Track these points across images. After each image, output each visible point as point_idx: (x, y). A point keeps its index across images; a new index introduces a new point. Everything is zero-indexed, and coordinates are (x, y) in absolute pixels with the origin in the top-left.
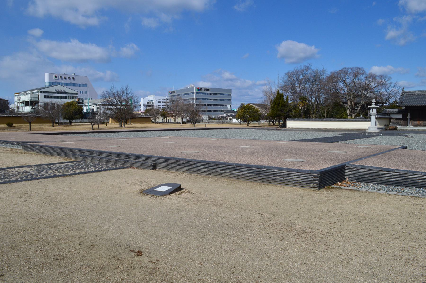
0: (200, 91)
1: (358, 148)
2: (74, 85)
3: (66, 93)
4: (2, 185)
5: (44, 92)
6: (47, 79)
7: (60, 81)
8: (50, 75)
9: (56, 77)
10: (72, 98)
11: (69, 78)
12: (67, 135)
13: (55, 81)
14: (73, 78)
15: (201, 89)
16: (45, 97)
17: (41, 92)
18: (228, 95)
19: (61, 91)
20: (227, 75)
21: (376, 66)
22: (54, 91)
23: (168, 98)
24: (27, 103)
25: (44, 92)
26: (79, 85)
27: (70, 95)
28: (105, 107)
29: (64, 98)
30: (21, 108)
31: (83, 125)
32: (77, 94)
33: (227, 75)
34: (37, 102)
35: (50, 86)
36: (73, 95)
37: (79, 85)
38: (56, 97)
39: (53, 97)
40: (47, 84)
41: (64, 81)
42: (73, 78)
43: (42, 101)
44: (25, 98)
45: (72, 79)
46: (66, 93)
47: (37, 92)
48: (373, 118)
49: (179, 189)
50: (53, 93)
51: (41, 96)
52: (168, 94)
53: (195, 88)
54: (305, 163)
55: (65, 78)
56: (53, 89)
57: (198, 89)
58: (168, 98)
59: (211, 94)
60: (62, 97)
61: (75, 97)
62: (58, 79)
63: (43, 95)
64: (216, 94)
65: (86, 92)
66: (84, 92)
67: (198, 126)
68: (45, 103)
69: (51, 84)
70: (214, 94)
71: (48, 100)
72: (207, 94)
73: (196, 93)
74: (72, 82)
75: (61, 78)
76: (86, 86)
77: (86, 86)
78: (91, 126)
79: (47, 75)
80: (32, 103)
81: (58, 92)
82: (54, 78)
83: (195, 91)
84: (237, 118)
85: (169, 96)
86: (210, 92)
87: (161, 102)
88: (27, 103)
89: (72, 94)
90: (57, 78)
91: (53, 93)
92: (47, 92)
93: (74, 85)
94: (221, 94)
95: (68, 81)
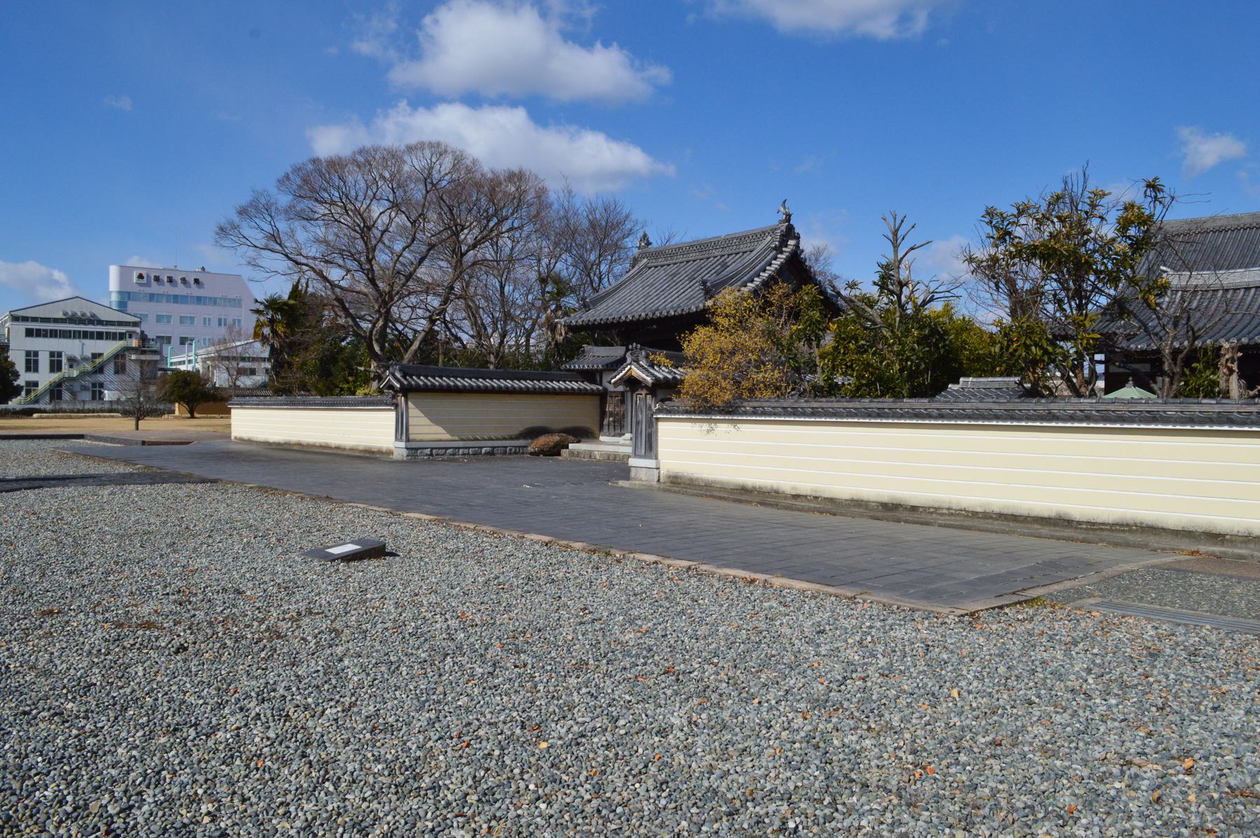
2: (199, 300)
3: (100, 322)
4: (1257, 532)
5: (25, 319)
6: (114, 285)
8: (125, 271)
9: (141, 276)
10: (122, 336)
13: (137, 289)
14: (197, 281)
16: (29, 333)
19: (84, 315)
22: (60, 315)
25: (25, 319)
26: (214, 301)
27: (112, 329)
29: (92, 338)
31: (71, 418)
36: (123, 329)
37: (214, 301)
39: (54, 334)
42: (197, 281)
46: (100, 322)
48: (273, 190)
60: (86, 335)
62: (148, 284)
63: (22, 327)
71: (44, 346)
74: (195, 291)
78: (133, 422)
79: (114, 271)
82: (135, 279)
89: (120, 324)
90: (145, 281)
91: (56, 321)
92: (35, 319)
93: (199, 300)
95: (180, 290)
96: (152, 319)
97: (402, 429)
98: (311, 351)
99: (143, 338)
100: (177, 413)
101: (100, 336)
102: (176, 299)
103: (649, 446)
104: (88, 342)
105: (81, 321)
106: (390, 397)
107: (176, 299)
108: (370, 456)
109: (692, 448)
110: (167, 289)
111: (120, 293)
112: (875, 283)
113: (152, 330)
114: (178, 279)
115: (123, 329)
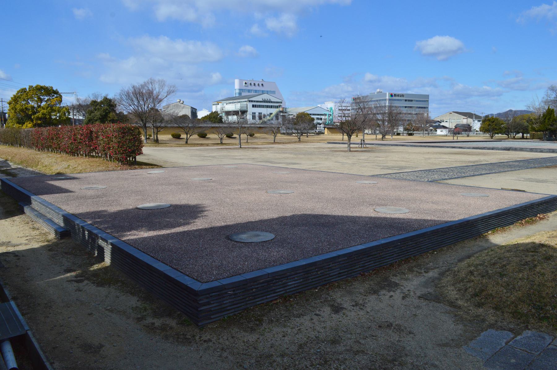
0: (394, 98)
1: (211, 296)
3: (272, 102)
5: (252, 101)
6: (237, 86)
7: (250, 88)
8: (241, 81)
9: (246, 83)
10: (277, 107)
14: (262, 85)
15: (395, 95)
16: (253, 106)
17: (250, 101)
18: (425, 101)
20: (369, 76)
25: (252, 101)
32: (281, 102)
33: (369, 76)
36: (277, 104)
40: (237, 91)
42: (262, 85)
45: (261, 85)
46: (272, 102)
47: (245, 101)
50: (260, 102)
51: (250, 105)
53: (387, 94)
54: (529, 237)
55: (254, 85)
56: (259, 98)
57: (392, 95)
59: (406, 100)
60: (267, 107)
61: (280, 106)
63: (252, 104)
64: (412, 101)
70: (409, 100)
71: (257, 110)
72: (401, 100)
73: (389, 100)
74: (261, 88)
79: (237, 82)
82: (244, 84)
83: (387, 98)
86: (404, 98)
89: (277, 102)
91: (260, 102)
92: (254, 101)
94: (417, 101)
95: (257, 88)
101: (271, 107)
104: (269, 109)
108: (6, 364)
111: (240, 89)
114: (257, 84)
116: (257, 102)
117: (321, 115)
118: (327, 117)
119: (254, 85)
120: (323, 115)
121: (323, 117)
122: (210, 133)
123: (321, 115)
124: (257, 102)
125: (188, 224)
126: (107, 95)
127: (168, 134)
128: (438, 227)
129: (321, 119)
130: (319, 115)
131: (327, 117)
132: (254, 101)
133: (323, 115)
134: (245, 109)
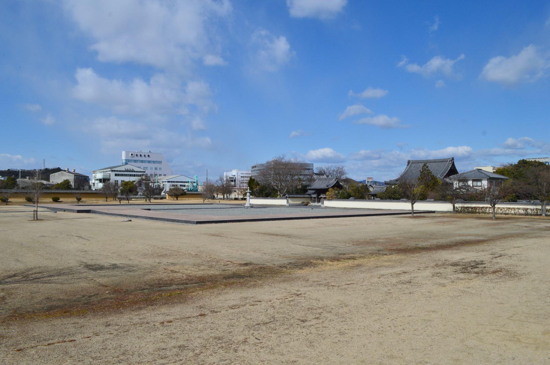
2: (149, 162)
3: (135, 172)
5: (115, 171)
6: (124, 157)
7: (136, 158)
8: (127, 153)
9: (132, 155)
11: (145, 156)
12: (238, 223)
14: (148, 156)
16: (116, 175)
17: (112, 171)
21: (450, 146)
23: (250, 172)
24: (100, 180)
25: (115, 171)
26: (154, 162)
28: (170, 183)
30: (96, 185)
34: (109, 180)
35: (126, 164)
36: (141, 173)
37: (154, 162)
38: (126, 175)
39: (122, 175)
40: (124, 161)
41: (139, 158)
42: (148, 156)
43: (113, 178)
44: (100, 176)
45: (147, 156)
46: (135, 172)
49: (131, 221)
50: (123, 171)
52: (250, 168)
55: (141, 156)
58: (250, 172)
60: (131, 175)
63: (114, 173)
65: (160, 169)
66: (158, 169)
67: (137, 197)
68: (115, 181)
69: (127, 162)
74: (147, 159)
75: (137, 155)
76: (160, 162)
77: (160, 162)
79: (124, 153)
80: (104, 180)
81: (127, 171)
84: (542, 201)
85: (252, 171)
87: (243, 177)
88: (100, 180)
89: (140, 172)
91: (123, 171)
92: (117, 171)
93: (149, 162)
95: (143, 158)
96: (149, 169)
97: (288, 202)
98: (260, 188)
99: (146, 176)
100: (167, 198)
101: (134, 175)
102: (142, 161)
103: (323, 204)
104: (131, 177)
105: (130, 171)
106: (284, 196)
107: (142, 161)
109: (327, 203)
110: (139, 158)
112: (343, 167)
113: (148, 172)
115: (141, 173)
116: (120, 171)
117: (185, 182)
118: (190, 184)
119: (141, 156)
120: (187, 182)
121: (186, 184)
122: (83, 197)
123: (185, 182)
124: (120, 171)
125: (462, 207)
126: (343, 167)
127: (50, 197)
128: (103, 278)
129: (184, 186)
130: (183, 182)
131: (190, 184)
132: (117, 171)
133: (187, 182)
134: (108, 177)
